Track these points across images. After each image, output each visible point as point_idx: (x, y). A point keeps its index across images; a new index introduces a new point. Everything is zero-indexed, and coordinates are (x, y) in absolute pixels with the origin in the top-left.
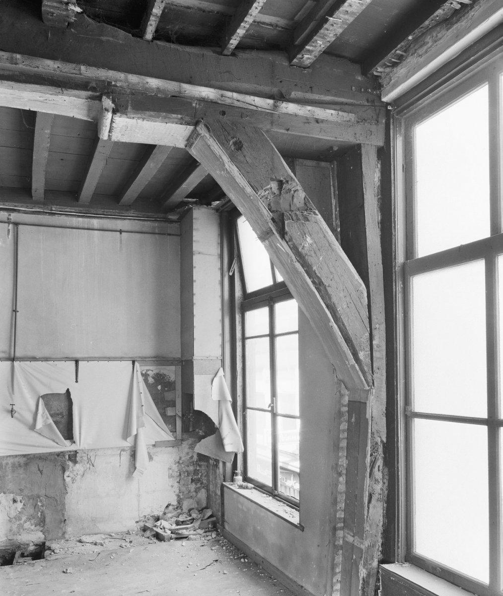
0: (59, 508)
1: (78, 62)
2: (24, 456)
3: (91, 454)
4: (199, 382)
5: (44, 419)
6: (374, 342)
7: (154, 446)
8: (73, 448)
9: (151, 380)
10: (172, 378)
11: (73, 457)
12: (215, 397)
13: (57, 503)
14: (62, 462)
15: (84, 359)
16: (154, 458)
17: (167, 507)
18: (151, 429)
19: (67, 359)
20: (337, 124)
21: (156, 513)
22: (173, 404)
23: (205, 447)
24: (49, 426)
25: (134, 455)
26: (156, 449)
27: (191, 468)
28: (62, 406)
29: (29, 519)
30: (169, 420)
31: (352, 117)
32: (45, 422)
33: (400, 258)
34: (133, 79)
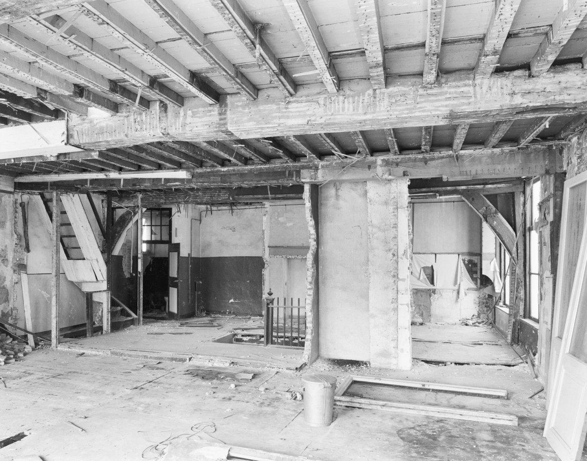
0: (428, 310)
1: (430, 187)
2: (416, 289)
3: (441, 291)
4: (485, 263)
5: (423, 276)
6: (519, 251)
7: (467, 289)
8: (434, 288)
9: (466, 262)
10: (476, 262)
11: (434, 291)
12: (492, 269)
13: (428, 308)
14: (431, 293)
15: (438, 254)
17: (473, 316)
18: (466, 282)
19: (432, 253)
20: (506, 188)
22: (476, 273)
23: (487, 290)
25: (458, 293)
27: (485, 301)
28: (429, 271)
29: (417, 313)
30: (474, 280)
31: (511, 185)
33: (528, 225)
34: (444, 188)
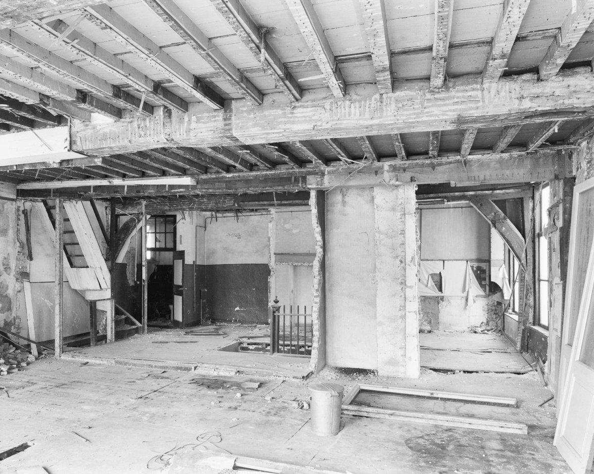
3: (449, 298)
4: (493, 270)
5: (431, 283)
7: (476, 297)
8: (442, 295)
9: (475, 269)
10: (485, 268)
11: (442, 299)
12: (501, 276)
13: (436, 316)
14: (439, 300)
16: (477, 302)
18: (475, 289)
19: (440, 260)
21: (477, 325)
23: (496, 297)
24: (433, 286)
25: (467, 300)
26: (477, 298)
27: (494, 308)
28: (437, 278)
30: (483, 286)
31: (520, 190)
32: (431, 284)
34: (452, 194)
